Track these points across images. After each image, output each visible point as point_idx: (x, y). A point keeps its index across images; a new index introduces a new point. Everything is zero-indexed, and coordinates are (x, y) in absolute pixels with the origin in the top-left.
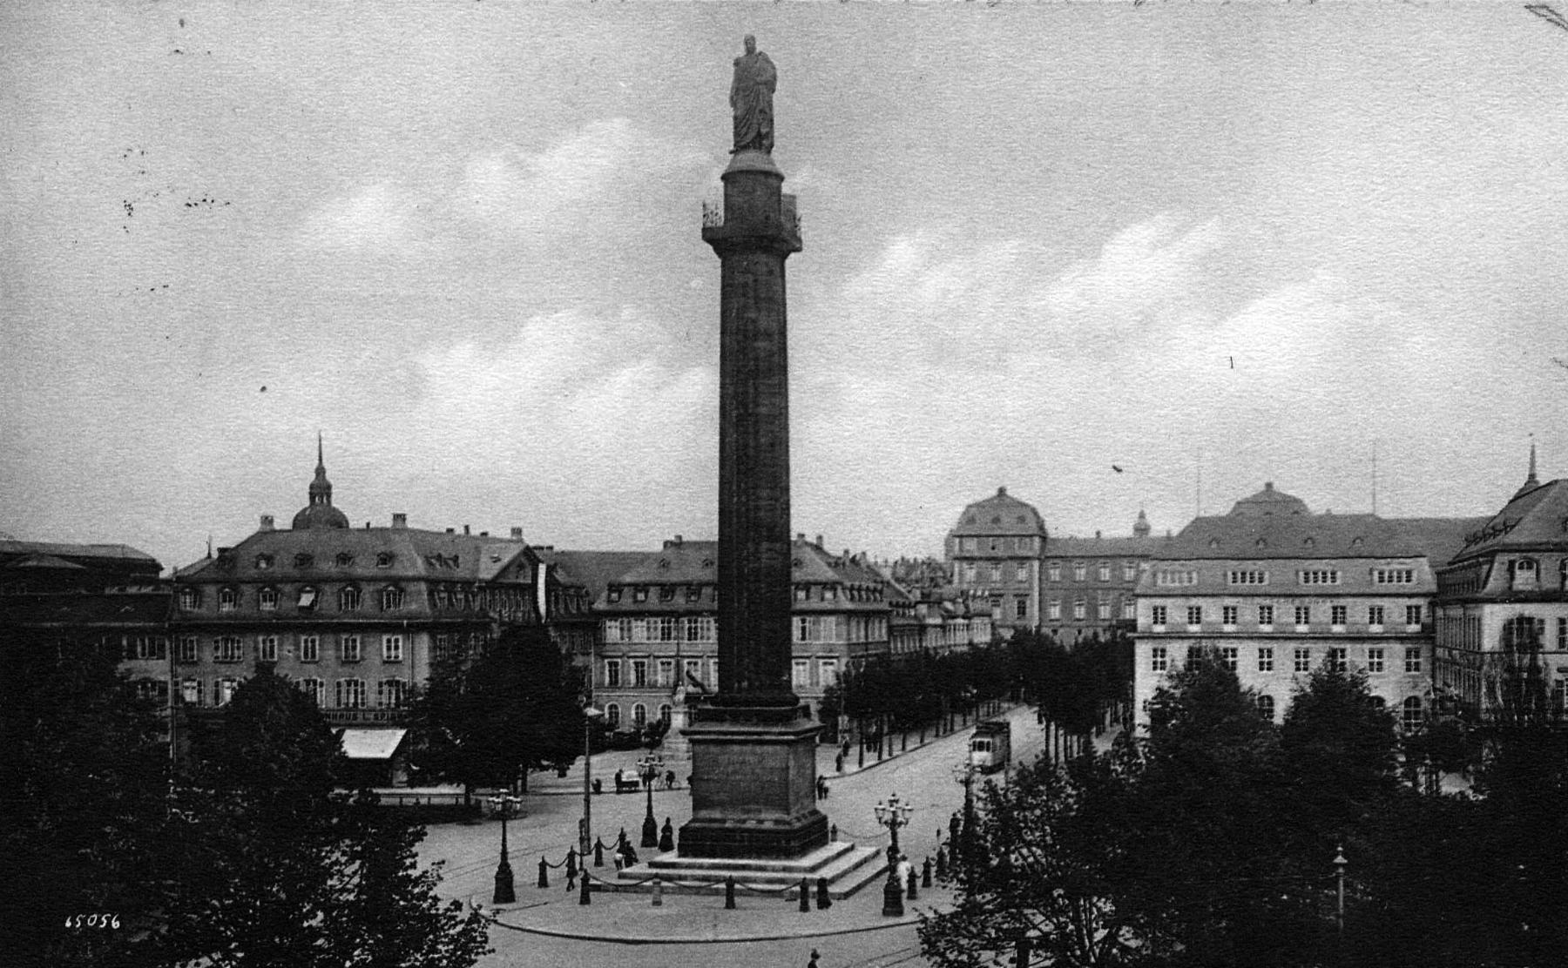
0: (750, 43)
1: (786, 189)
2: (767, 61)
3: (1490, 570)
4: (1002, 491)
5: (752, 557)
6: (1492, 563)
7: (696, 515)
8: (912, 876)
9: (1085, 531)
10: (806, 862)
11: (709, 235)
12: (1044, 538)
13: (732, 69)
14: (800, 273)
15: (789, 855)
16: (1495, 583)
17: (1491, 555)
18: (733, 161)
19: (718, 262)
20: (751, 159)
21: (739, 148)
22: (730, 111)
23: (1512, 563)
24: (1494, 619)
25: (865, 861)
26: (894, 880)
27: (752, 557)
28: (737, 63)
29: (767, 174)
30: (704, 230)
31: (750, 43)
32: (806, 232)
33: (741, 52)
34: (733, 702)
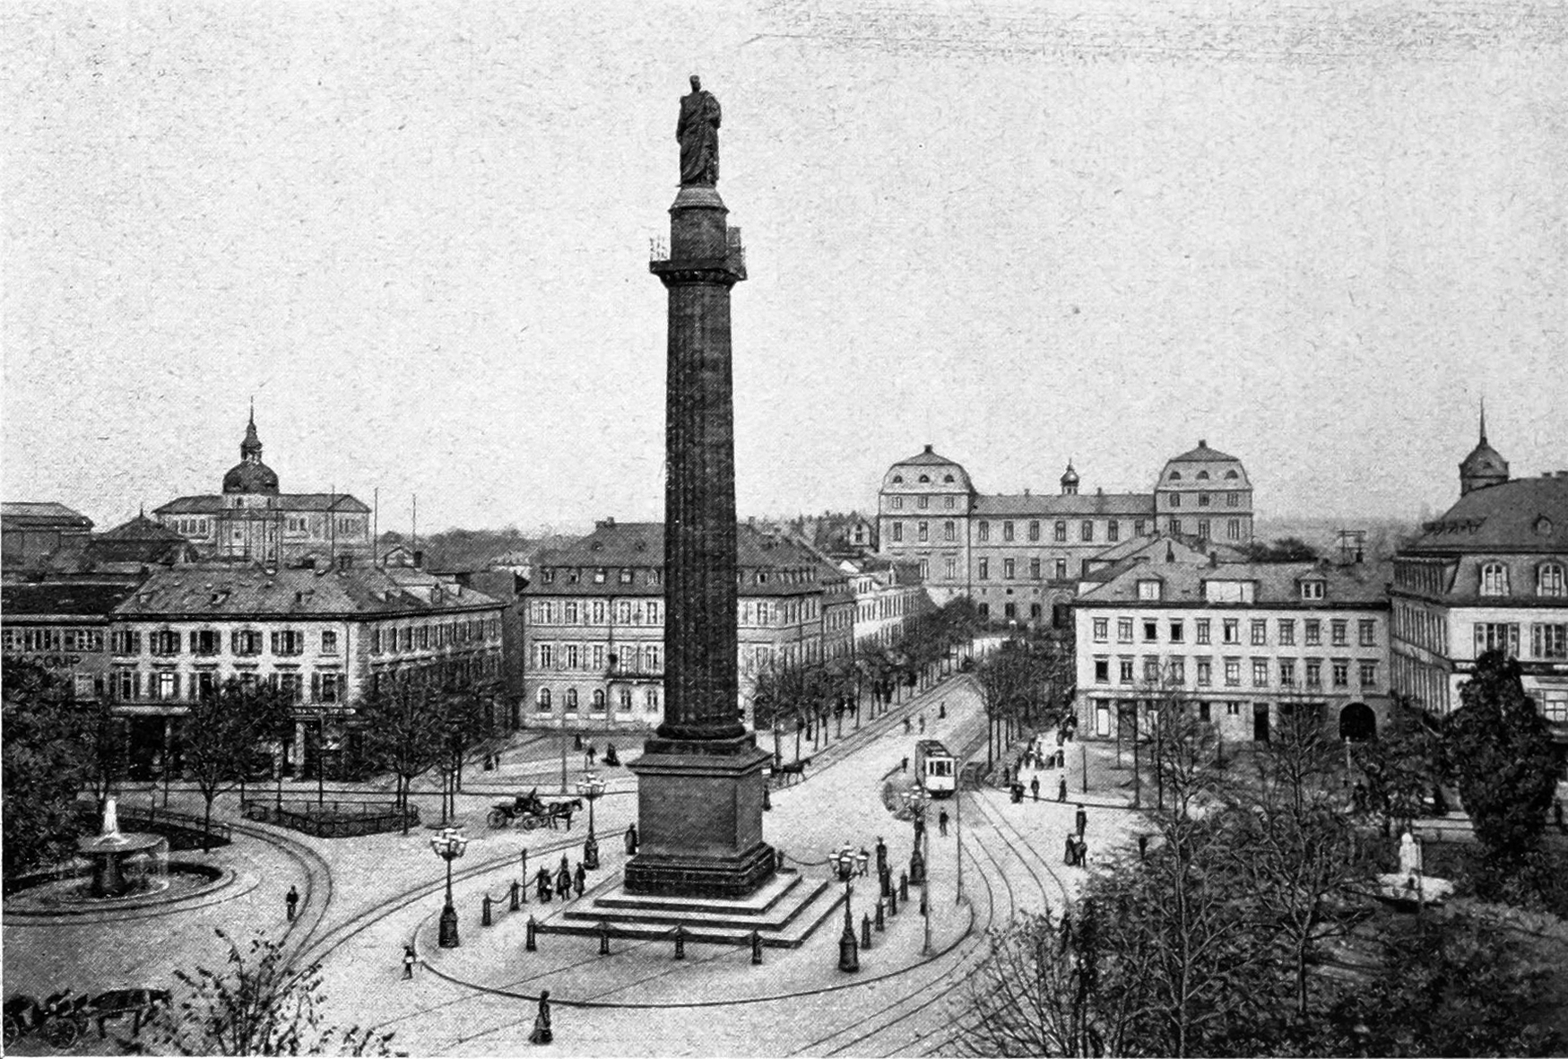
0: (695, 83)
1: (731, 221)
2: (713, 99)
3: (1456, 571)
4: (928, 449)
5: (698, 547)
6: (1457, 563)
7: (645, 501)
8: (866, 923)
9: (1012, 488)
10: (758, 901)
11: (656, 268)
12: (973, 495)
13: (679, 106)
14: (743, 303)
15: (737, 893)
16: (1462, 585)
17: (1455, 556)
18: (679, 196)
19: (665, 292)
20: (699, 194)
21: (687, 181)
22: (678, 147)
23: (1479, 568)
24: (1462, 635)
25: (815, 895)
26: (848, 931)
27: (698, 547)
28: (683, 100)
29: (714, 209)
30: (653, 264)
31: (695, 83)
32: (750, 261)
33: (688, 90)
34: (680, 734)
